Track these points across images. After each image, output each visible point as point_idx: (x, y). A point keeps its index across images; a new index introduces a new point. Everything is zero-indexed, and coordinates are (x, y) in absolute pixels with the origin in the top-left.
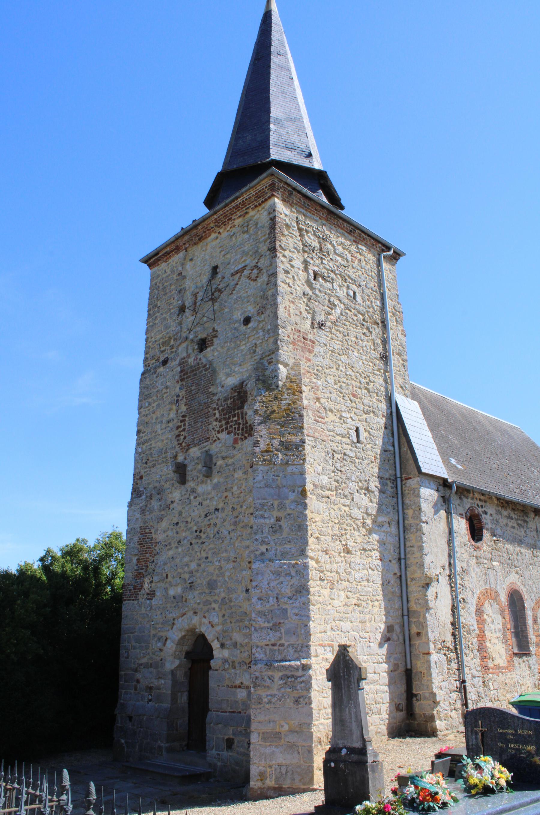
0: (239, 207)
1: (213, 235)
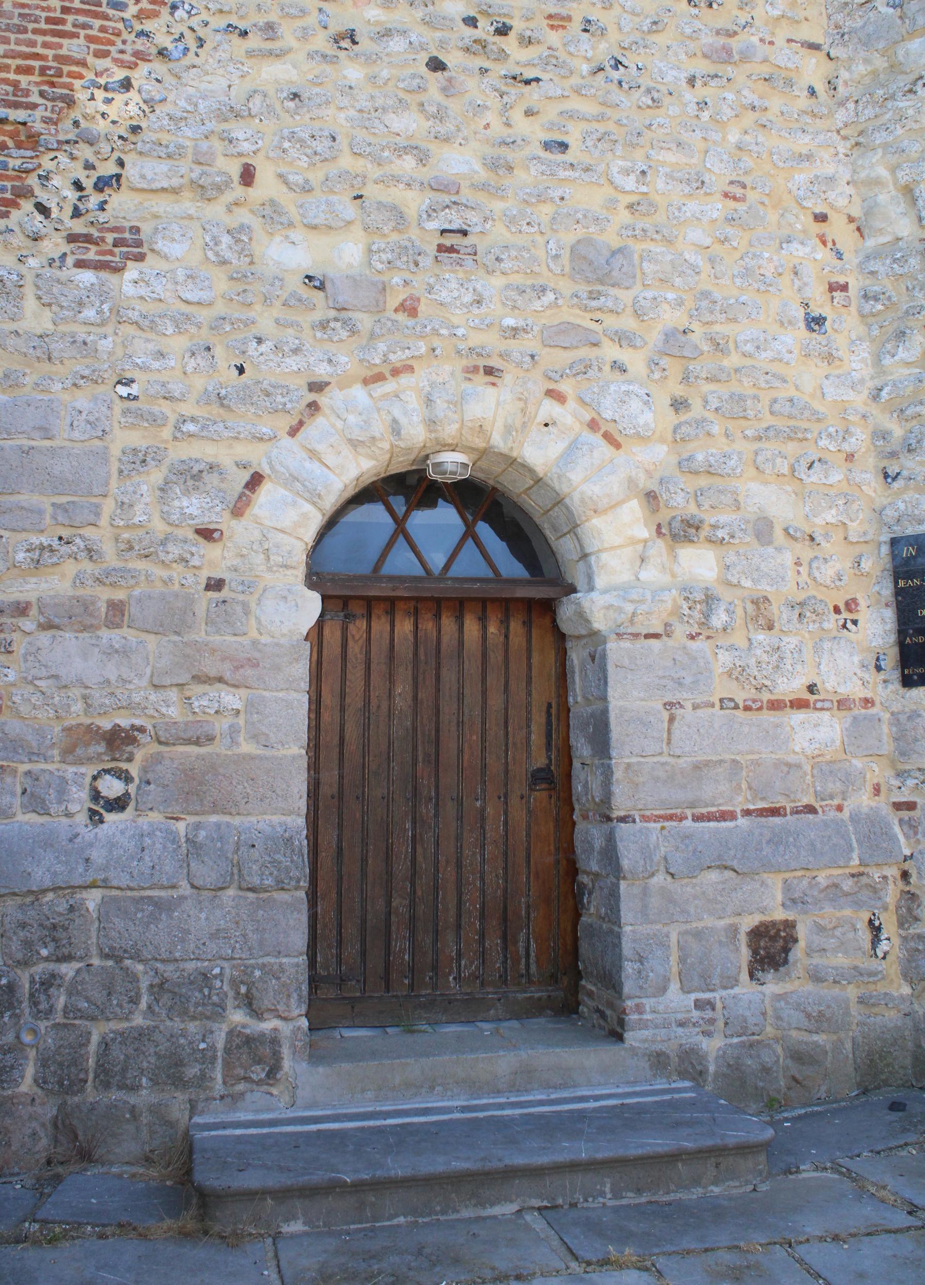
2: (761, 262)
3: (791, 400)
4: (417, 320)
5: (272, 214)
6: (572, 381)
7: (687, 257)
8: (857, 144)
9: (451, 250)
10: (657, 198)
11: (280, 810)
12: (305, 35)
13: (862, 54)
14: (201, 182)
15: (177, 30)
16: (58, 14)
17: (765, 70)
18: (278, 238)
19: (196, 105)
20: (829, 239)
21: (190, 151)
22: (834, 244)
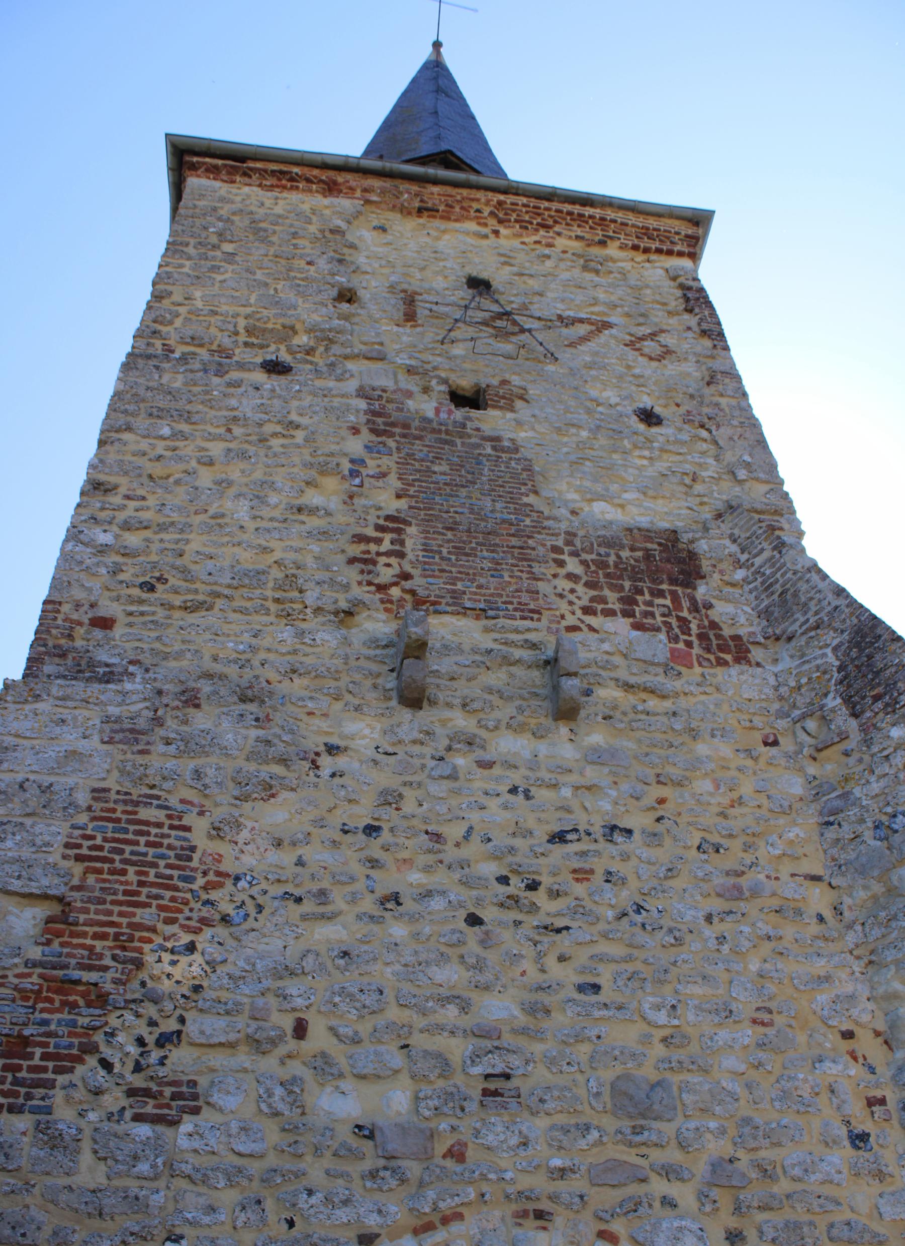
0: (587, 222)
1: (472, 226)
2: (796, 1083)
3: (848, 1224)
4: (465, 1165)
5: (323, 1066)
6: (623, 1219)
7: (725, 1085)
8: (871, 962)
9: (496, 1093)
10: (689, 1030)
12: (354, 899)
13: (861, 882)
14: (256, 1037)
15: (239, 897)
16: (134, 887)
17: (775, 903)
18: (329, 1089)
19: (254, 965)
20: (859, 1055)
21: (247, 1007)
22: (865, 1059)
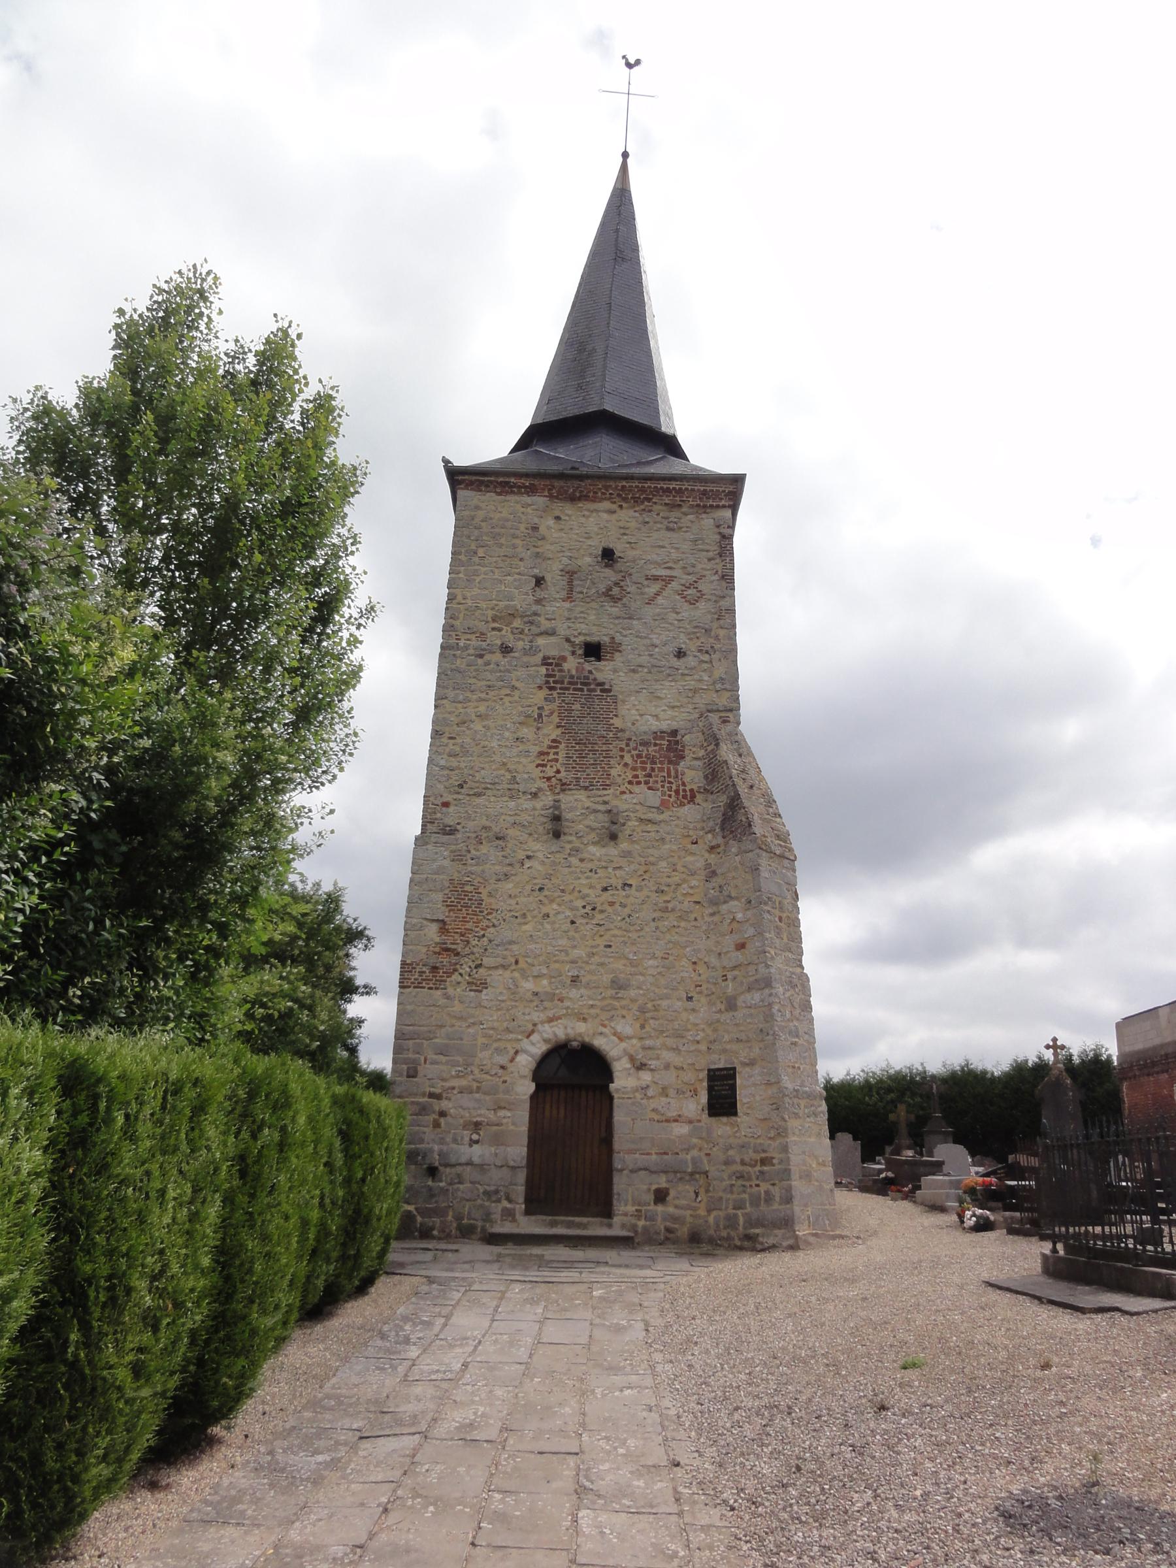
1: (606, 505)
11: (518, 1152)
